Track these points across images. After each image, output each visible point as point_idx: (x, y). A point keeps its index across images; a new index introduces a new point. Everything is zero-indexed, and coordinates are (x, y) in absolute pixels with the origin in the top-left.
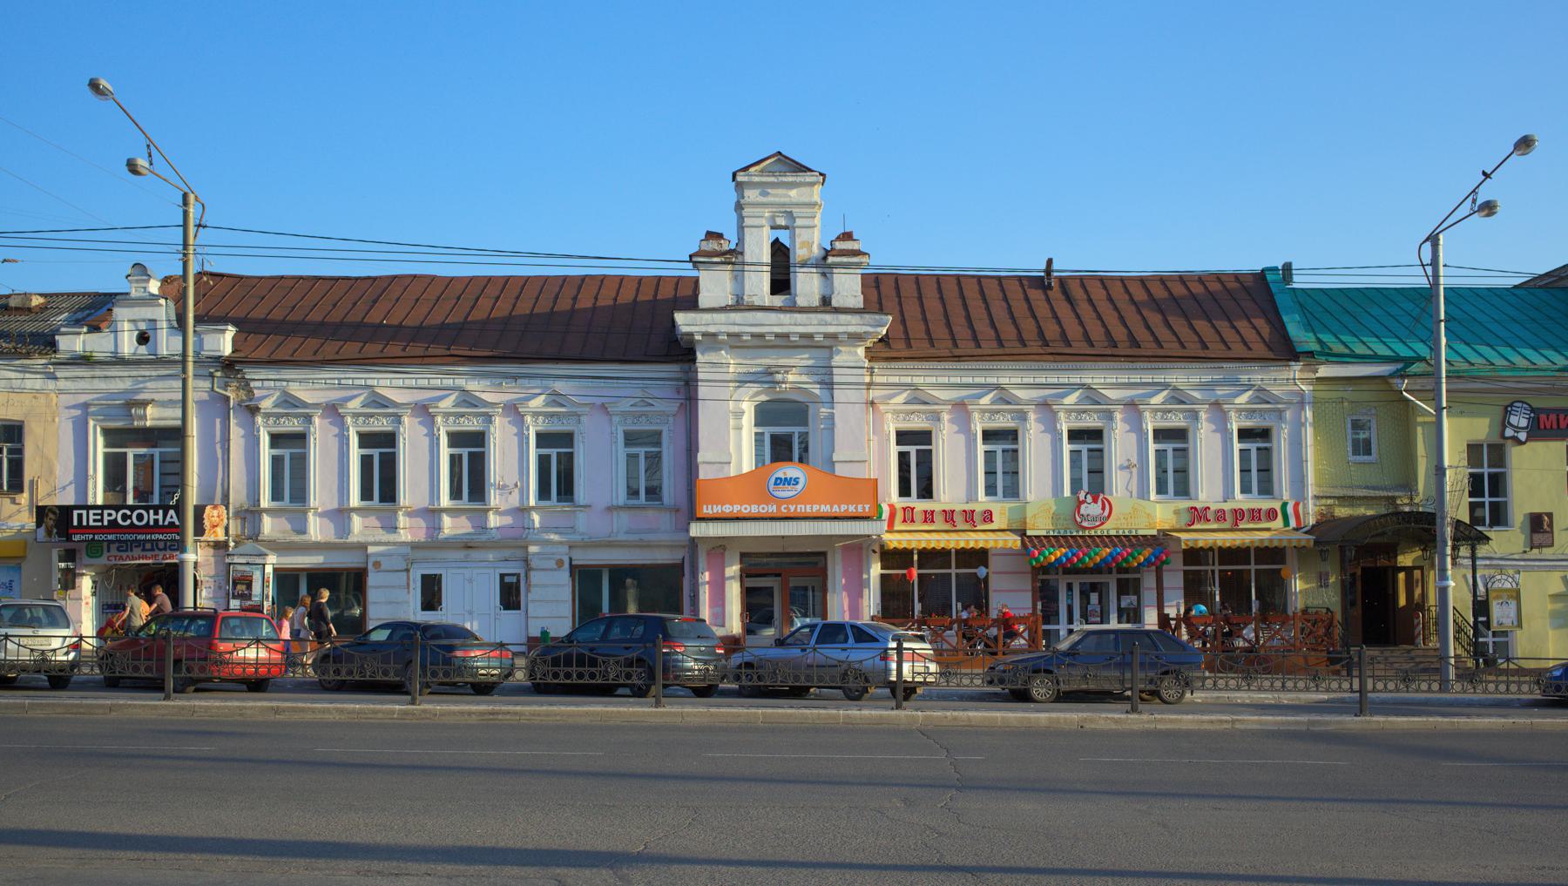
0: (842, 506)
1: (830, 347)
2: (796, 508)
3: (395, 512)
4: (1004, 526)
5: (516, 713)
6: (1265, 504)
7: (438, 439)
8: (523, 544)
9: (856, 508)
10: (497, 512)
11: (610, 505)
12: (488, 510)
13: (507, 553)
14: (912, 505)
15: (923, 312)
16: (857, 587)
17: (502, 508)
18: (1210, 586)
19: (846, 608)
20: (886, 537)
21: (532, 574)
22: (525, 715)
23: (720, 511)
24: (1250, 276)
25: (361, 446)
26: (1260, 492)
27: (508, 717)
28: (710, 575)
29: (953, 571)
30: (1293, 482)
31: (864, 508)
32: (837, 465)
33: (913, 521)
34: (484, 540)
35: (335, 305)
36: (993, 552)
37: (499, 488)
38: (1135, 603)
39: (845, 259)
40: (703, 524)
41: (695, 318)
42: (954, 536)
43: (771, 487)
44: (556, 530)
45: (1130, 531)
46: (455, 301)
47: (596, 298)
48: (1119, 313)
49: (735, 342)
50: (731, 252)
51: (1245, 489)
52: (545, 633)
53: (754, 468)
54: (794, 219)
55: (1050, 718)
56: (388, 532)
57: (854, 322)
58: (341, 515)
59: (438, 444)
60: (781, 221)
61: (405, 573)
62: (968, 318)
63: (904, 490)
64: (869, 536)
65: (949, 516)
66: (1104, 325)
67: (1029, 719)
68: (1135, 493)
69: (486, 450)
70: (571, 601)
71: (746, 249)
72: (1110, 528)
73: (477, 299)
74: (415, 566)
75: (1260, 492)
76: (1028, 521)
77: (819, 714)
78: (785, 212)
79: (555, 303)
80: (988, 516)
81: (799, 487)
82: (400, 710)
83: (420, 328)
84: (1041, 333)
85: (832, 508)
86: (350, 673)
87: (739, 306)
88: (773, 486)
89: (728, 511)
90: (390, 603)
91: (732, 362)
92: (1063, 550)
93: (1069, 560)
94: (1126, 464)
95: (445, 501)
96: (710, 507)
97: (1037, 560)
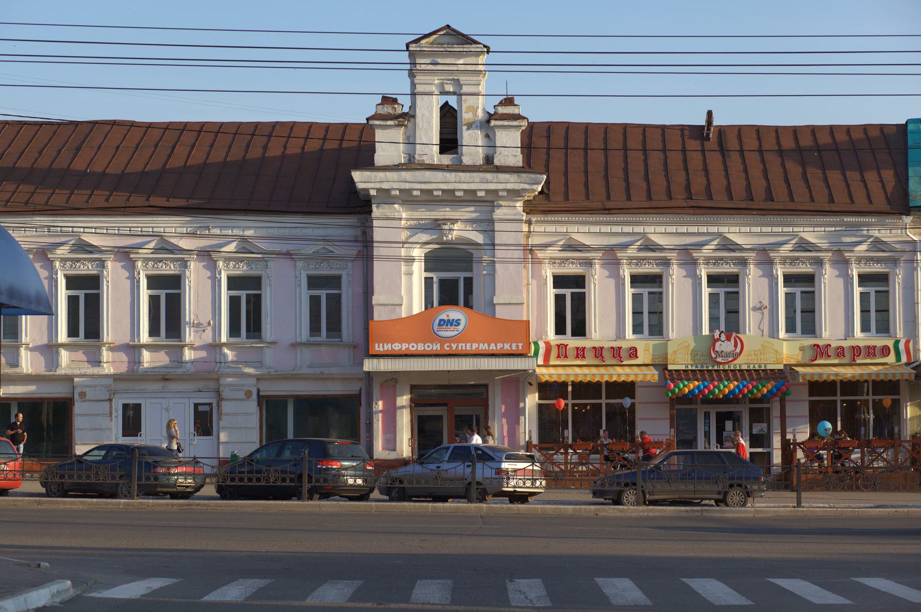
0: (498, 344)
1: (493, 202)
2: (457, 346)
3: (99, 348)
4: (647, 362)
5: (204, 505)
6: (880, 342)
7: (138, 282)
8: (214, 376)
9: (511, 346)
10: (192, 347)
11: (293, 341)
12: (184, 346)
13: (201, 385)
14: (565, 342)
15: (586, 164)
16: (515, 414)
17: (197, 344)
18: (864, 413)
19: (505, 433)
20: (539, 371)
21: (223, 403)
22: (211, 506)
23: (390, 349)
24: (894, 127)
25: (67, 288)
26: (878, 331)
27: (199, 507)
28: (384, 405)
29: (604, 401)
30: (906, 322)
31: (518, 346)
32: (497, 307)
33: (566, 357)
34: (180, 373)
35: (40, 153)
36: (639, 385)
37: (193, 326)
38: (765, 430)
39: (506, 123)
40: (375, 361)
41: (370, 177)
42: (602, 370)
43: (436, 327)
44: (247, 363)
45: (760, 366)
46: (153, 149)
47: (285, 147)
48: (764, 165)
49: (407, 198)
50: (404, 115)
51: (865, 328)
52: (234, 456)
53: (423, 310)
54: (461, 86)
55: (575, 509)
56: (93, 366)
57: (512, 180)
58: (50, 350)
59: (138, 287)
60: (450, 88)
61: (107, 404)
62: (626, 170)
63: (560, 329)
64: (525, 370)
65: (598, 352)
66: (747, 178)
67: (560, 509)
68: (766, 332)
69: (182, 291)
70: (258, 428)
71: (417, 113)
72: (742, 363)
73: (174, 147)
74: (117, 396)
75: (878, 331)
76: (669, 356)
77: (415, 506)
78: (453, 80)
79: (246, 151)
80: (633, 352)
81: (461, 327)
82: (124, 503)
83: (122, 176)
84: (688, 187)
85: (489, 346)
86: (88, 477)
87: (411, 164)
88: (437, 327)
89: (397, 349)
90: (95, 429)
91: (404, 215)
92: (696, 383)
93: (741, 391)
94: (758, 305)
95: (144, 337)
96: (381, 345)
97: (673, 391)
